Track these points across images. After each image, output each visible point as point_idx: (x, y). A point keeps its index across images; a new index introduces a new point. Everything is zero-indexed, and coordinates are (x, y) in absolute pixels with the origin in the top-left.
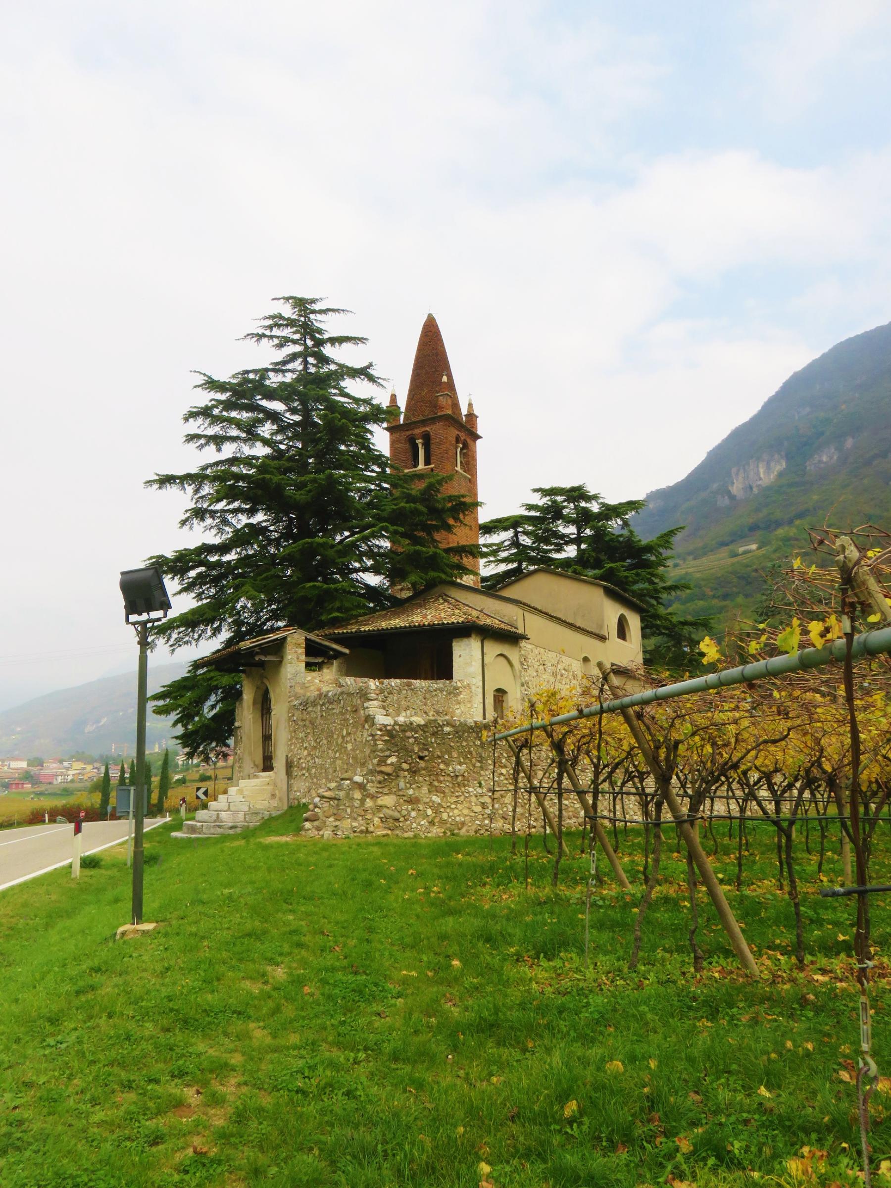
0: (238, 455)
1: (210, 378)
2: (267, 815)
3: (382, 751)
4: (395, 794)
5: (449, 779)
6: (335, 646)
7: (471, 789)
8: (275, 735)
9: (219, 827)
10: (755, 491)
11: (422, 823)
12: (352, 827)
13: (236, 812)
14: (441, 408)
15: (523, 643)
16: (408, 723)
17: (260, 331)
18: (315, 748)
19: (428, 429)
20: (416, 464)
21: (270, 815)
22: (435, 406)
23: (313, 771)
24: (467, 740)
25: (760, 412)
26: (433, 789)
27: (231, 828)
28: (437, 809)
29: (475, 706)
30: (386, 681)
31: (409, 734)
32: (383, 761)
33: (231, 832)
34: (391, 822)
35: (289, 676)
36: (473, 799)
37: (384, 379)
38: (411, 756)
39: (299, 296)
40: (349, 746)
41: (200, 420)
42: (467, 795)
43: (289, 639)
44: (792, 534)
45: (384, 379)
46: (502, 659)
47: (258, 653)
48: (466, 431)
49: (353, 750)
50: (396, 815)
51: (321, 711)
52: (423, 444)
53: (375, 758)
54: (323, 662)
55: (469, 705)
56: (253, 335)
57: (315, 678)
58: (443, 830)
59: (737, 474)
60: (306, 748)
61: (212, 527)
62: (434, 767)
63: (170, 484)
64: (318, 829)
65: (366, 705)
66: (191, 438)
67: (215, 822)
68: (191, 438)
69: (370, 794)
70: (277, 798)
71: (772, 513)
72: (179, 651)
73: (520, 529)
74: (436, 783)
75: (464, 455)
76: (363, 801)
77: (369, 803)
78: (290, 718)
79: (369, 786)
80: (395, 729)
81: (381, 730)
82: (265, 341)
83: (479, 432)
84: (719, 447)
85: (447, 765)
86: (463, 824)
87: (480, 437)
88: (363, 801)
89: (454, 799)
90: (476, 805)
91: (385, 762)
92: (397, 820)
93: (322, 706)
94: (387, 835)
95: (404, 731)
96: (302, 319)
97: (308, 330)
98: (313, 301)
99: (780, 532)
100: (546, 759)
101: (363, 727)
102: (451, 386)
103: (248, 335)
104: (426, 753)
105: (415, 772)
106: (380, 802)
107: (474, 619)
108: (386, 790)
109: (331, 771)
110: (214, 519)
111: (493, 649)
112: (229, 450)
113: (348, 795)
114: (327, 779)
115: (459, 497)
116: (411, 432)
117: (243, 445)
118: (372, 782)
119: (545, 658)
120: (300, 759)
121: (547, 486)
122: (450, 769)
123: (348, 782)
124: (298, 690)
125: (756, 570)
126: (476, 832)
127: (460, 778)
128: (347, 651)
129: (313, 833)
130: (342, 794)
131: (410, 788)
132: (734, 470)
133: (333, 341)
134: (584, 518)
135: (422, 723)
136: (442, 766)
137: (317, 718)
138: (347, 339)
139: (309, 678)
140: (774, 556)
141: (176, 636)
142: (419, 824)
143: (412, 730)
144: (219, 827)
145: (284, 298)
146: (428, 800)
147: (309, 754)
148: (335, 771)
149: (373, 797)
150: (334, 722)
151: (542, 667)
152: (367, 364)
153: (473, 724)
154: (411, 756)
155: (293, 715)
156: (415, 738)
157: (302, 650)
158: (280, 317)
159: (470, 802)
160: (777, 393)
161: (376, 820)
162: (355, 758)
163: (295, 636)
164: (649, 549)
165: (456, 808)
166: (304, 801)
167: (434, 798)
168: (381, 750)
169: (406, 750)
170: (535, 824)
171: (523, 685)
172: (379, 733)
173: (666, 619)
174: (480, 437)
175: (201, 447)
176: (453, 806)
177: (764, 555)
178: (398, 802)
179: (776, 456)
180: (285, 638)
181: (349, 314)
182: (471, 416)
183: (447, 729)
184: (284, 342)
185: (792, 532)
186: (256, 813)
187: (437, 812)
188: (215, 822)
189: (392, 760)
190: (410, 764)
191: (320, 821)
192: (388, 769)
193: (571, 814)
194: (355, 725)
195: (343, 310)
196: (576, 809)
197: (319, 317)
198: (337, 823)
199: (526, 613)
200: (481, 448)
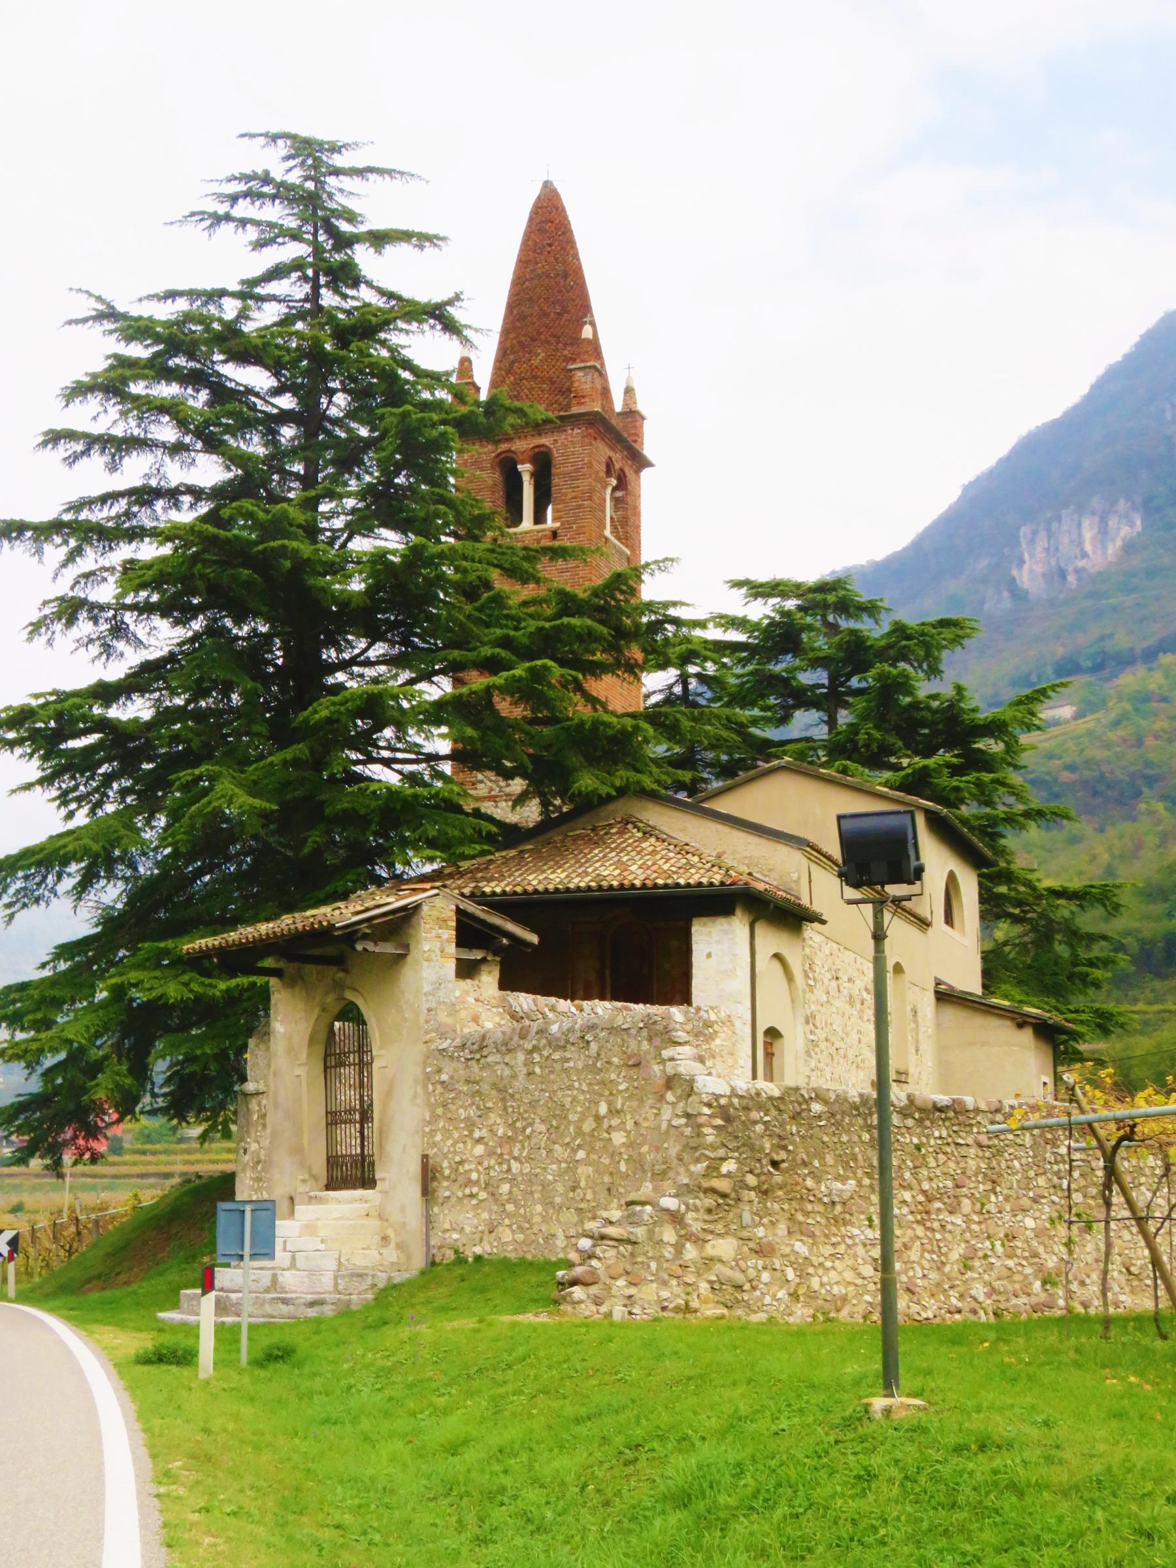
0: (153, 483)
1: (109, 306)
2: (382, 1280)
3: (713, 1147)
4: (734, 1235)
5: (821, 1208)
6: (511, 927)
7: (856, 1231)
8: (383, 1112)
9: (285, 1301)
10: (1071, 578)
11: (780, 1295)
12: (660, 1300)
13: (313, 1272)
14: (580, 398)
15: (811, 931)
16: (753, 1092)
17: (222, 209)
18: (510, 1140)
19: (546, 441)
20: (517, 519)
21: (390, 1278)
22: (564, 390)
23: (505, 1188)
24: (848, 1132)
25: (1089, 399)
26: (797, 1229)
27: (312, 1304)
28: (803, 1267)
29: (741, 1062)
30: (586, 1004)
31: (755, 1115)
32: (713, 1169)
33: (312, 1313)
34: (732, 1291)
35: (427, 988)
36: (860, 1250)
37: (476, 330)
38: (759, 1160)
39: (304, 133)
40: (619, 1138)
41: (94, 402)
42: (849, 1242)
43: (425, 908)
44: (1153, 687)
45: (476, 330)
46: (776, 964)
47: (365, 937)
48: (620, 440)
49: (630, 1145)
50: (739, 1277)
51: (529, 1063)
52: (533, 475)
53: (697, 1161)
54: (484, 960)
55: (730, 1061)
56: (201, 215)
57: (466, 993)
58: (812, 1311)
59: (1032, 541)
60: (480, 1140)
61: (91, 641)
62: (797, 1184)
63: (10, 540)
64: (598, 1301)
65: (666, 1054)
66: (54, 437)
67: (267, 1291)
68: (54, 437)
69: (692, 1234)
70: (392, 1245)
71: (1111, 636)
72: (22, 917)
73: (692, 669)
74: (800, 1217)
75: (618, 502)
76: (679, 1248)
77: (691, 1252)
78: (428, 1077)
79: (690, 1216)
80: (732, 1104)
81: (709, 1105)
82: (227, 228)
83: (649, 449)
84: (991, 476)
85: (818, 1180)
86: (844, 1299)
87: (648, 464)
88: (679, 1248)
89: (828, 1250)
90: (865, 1263)
91: (717, 1169)
92: (739, 1287)
93: (531, 1052)
94: (722, 1317)
95: (746, 1109)
96: (310, 185)
97: (311, 204)
98: (335, 149)
99: (1130, 680)
100: (976, 1175)
101: (661, 1098)
102: (594, 348)
103: (193, 214)
104: (782, 1155)
105: (765, 1193)
106: (710, 1250)
107: (745, 878)
108: (719, 1227)
109: (560, 1187)
110: (96, 623)
111: (770, 940)
112: (136, 470)
113: (651, 1233)
114: (548, 1203)
115: (666, 605)
116: (503, 447)
117: (167, 459)
118: (696, 1210)
119: (839, 965)
120: (461, 1163)
121: (763, 576)
122: (823, 1188)
123: (648, 1208)
124: (443, 1018)
125: (1072, 768)
126: (865, 1318)
127: (839, 1208)
128: (534, 939)
129: (587, 1309)
130: (640, 1232)
131: (760, 1224)
132: (1025, 531)
133: (379, 239)
134: (856, 654)
135: (776, 1093)
136: (809, 1183)
137: (514, 1076)
138: (405, 236)
139: (458, 993)
140: (1112, 736)
141: (19, 884)
142: (774, 1297)
143: (760, 1107)
144: (285, 1301)
145: (266, 135)
146: (787, 1250)
147: (491, 1153)
148: (573, 1189)
149: (700, 1241)
150: (571, 1088)
151: (834, 984)
152: (451, 295)
153: (857, 1100)
154: (759, 1160)
155: (439, 1071)
156: (765, 1123)
157: (450, 934)
158: (266, 179)
159: (855, 1256)
160: (1127, 357)
161: (704, 1287)
162: (638, 1164)
163: (438, 902)
164: (995, 728)
165: (833, 1268)
166: (478, 1250)
167: (798, 1246)
168: (711, 1145)
169: (752, 1148)
170: (960, 1305)
171: (807, 1022)
172: (706, 1110)
173: (1028, 884)
174: (648, 464)
175: (74, 458)
176: (828, 1264)
177: (1090, 733)
178: (739, 1251)
179: (1122, 505)
180: (417, 907)
181: (414, 183)
182: (632, 416)
183: (817, 1107)
184: (270, 235)
185: (1155, 681)
186: (360, 1275)
187: (803, 1275)
188: (267, 1291)
189: (729, 1166)
190: (758, 1176)
191: (600, 1286)
192: (723, 1185)
193: (1017, 1286)
194: (638, 1095)
195: (402, 173)
196: (1026, 1276)
197: (345, 182)
198: (633, 1291)
199: (813, 867)
200: (648, 483)
